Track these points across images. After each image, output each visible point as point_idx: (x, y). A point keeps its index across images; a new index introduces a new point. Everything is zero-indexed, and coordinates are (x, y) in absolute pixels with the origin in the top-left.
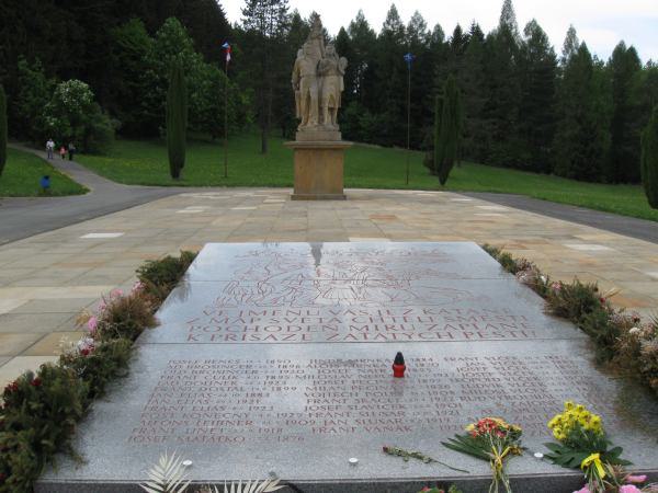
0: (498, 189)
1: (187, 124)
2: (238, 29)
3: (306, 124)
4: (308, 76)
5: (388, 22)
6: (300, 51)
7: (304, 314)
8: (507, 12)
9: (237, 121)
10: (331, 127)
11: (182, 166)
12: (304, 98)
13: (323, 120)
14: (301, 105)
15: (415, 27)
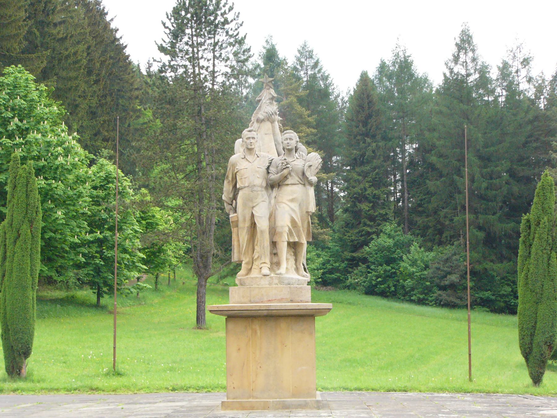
0: (188, 380)
1: (39, 266)
2: (158, 78)
3: (250, 270)
4: (251, 187)
5: (456, 59)
6: (238, 142)
9: (144, 262)
10: (293, 275)
11: (26, 353)
12: (244, 225)
13: (278, 264)
14: (240, 237)
15: (516, 65)
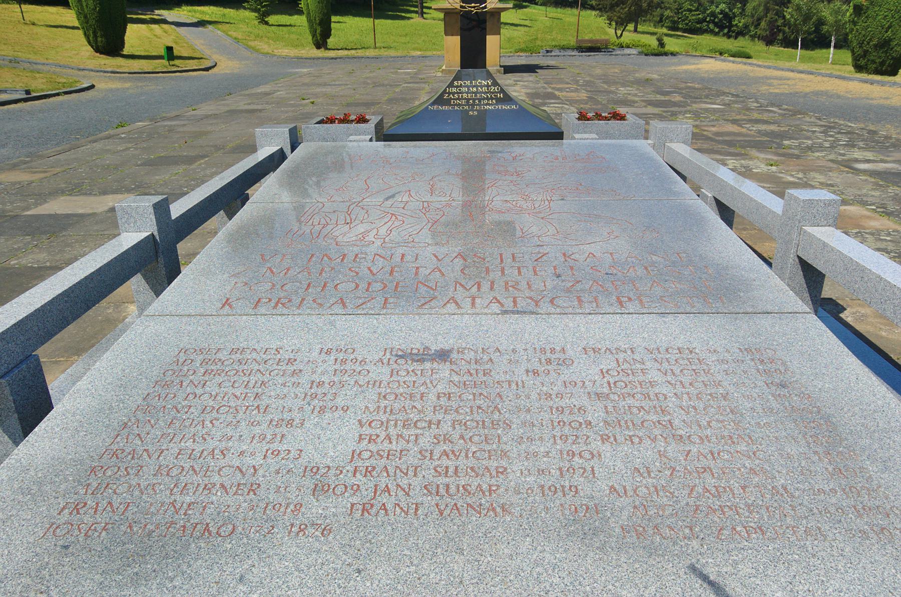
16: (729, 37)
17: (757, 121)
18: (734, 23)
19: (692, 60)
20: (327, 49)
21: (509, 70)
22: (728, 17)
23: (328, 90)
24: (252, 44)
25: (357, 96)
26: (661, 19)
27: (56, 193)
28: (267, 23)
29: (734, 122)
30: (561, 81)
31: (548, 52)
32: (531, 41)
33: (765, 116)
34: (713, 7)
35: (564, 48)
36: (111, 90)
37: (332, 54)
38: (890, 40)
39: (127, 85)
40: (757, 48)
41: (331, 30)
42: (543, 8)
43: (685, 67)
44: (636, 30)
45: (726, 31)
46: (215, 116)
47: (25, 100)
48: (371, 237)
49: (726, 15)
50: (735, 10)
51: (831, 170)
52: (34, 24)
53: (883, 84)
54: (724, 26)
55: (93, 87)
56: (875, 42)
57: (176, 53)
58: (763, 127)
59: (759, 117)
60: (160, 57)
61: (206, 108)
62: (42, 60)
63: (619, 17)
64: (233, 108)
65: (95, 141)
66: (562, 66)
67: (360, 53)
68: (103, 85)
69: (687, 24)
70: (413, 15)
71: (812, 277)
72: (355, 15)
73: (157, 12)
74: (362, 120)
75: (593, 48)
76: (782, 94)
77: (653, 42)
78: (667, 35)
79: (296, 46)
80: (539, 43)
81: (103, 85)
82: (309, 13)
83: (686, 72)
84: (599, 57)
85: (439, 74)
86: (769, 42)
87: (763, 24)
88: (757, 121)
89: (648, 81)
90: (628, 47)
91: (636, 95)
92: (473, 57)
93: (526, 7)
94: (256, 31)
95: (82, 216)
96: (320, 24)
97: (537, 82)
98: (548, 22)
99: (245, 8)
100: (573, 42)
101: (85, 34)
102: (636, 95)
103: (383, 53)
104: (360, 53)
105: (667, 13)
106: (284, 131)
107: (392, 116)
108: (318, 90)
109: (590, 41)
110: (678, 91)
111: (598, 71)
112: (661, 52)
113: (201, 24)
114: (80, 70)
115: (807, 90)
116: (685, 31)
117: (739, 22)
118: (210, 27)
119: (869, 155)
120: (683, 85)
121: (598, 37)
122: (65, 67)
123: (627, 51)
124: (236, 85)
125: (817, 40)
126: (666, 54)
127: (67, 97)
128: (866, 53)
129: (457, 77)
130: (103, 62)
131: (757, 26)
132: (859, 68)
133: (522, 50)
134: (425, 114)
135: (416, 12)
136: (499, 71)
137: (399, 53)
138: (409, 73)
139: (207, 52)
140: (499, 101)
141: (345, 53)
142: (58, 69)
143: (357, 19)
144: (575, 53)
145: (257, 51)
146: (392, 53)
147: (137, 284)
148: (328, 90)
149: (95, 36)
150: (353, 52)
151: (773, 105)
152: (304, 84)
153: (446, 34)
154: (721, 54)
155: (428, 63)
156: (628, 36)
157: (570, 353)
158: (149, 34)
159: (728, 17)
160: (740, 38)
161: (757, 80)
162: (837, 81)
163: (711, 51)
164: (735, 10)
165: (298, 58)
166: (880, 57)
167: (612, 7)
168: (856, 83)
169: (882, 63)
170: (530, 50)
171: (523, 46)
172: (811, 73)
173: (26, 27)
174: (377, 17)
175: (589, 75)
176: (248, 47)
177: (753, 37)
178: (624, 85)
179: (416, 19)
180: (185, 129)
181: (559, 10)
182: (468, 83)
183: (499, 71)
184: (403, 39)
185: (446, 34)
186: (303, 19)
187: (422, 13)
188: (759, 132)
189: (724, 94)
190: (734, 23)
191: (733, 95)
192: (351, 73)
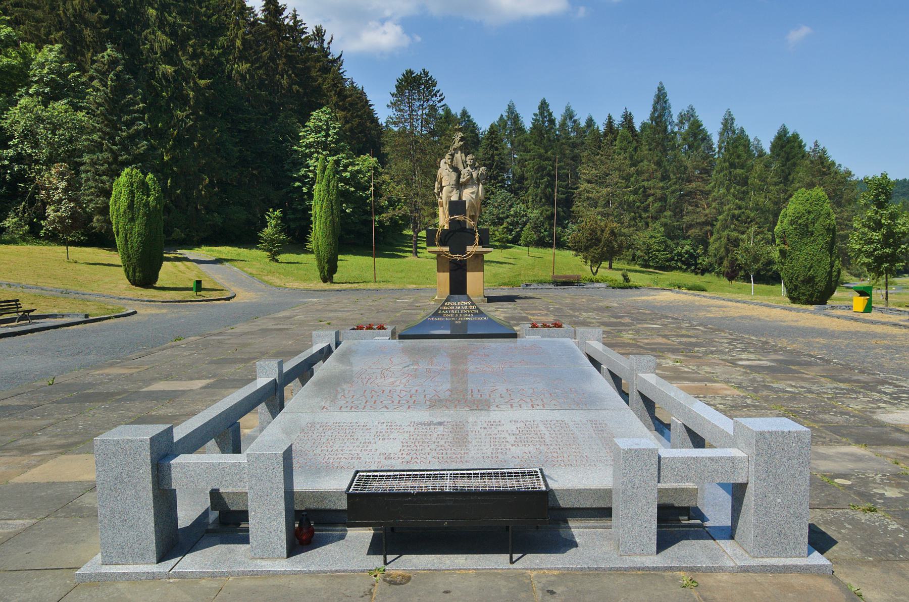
7: (413, 391)
8: (661, 98)
16: (697, 273)
17: (682, 336)
18: (699, 262)
19: (652, 292)
20: (332, 282)
21: (491, 299)
22: (693, 257)
23: (340, 314)
24: (266, 278)
25: (365, 319)
26: (634, 258)
27: (154, 380)
28: (277, 261)
29: (665, 336)
30: (535, 308)
31: (527, 285)
32: (515, 277)
33: (691, 333)
34: (679, 249)
35: (541, 282)
36: (152, 315)
37: (337, 287)
38: (814, 277)
39: (164, 311)
40: (722, 283)
41: (337, 267)
42: (526, 248)
43: (643, 298)
44: (610, 267)
45: (693, 268)
46: (252, 333)
47: (85, 322)
48: (398, 383)
49: (691, 255)
50: (698, 251)
51: (718, 365)
52: (76, 262)
53: (798, 310)
54: (690, 263)
55: (135, 312)
56: (801, 278)
57: (204, 285)
58: (684, 340)
59: (686, 333)
60: (191, 289)
61: (240, 328)
62: (87, 291)
63: (594, 257)
64: (264, 327)
65: (163, 349)
66: (538, 296)
67: (362, 286)
68: (144, 311)
69: (657, 262)
70: (408, 254)
71: (649, 404)
72: (355, 254)
73: (179, 251)
74: (381, 328)
75: (567, 283)
76: (715, 318)
77: (618, 277)
78: (630, 271)
79: (305, 280)
80: (522, 278)
81: (144, 311)
82: (318, 254)
83: (644, 301)
84: (572, 289)
85: (433, 303)
86: (731, 276)
87: (726, 263)
88: (682, 336)
89: (608, 308)
90: (598, 282)
91: (594, 318)
92: (458, 287)
93: (510, 247)
94: (268, 268)
95: (184, 391)
96: (328, 262)
97: (515, 309)
98: (530, 260)
99: (257, 248)
100: (549, 278)
101: (126, 270)
102: (594, 318)
103: (383, 286)
104: (362, 286)
105: (639, 253)
106: (333, 333)
107: (400, 329)
108: (331, 315)
109: (565, 277)
110: (629, 315)
111: (568, 301)
112: (626, 285)
113: (219, 261)
114: (120, 299)
115: (736, 315)
116: (656, 268)
117: (704, 261)
118: (227, 264)
119: (752, 357)
120: (636, 311)
121: (576, 273)
122: (108, 297)
123: (597, 285)
124: (253, 312)
125: (766, 276)
126: (631, 287)
127: (116, 320)
128: (796, 287)
129: (447, 300)
130: (139, 293)
131: (720, 264)
132: (794, 300)
133: (505, 284)
134: (425, 323)
135: (411, 252)
136: (483, 301)
137: (397, 287)
138: (404, 302)
139: (226, 285)
140: (475, 314)
141: (349, 286)
142: (102, 299)
143: (358, 258)
144: (552, 286)
145: (271, 284)
146: (391, 286)
147: (262, 408)
148: (340, 314)
149: (134, 272)
150: (356, 285)
151: (701, 325)
152: (317, 310)
153: (438, 271)
154: (679, 287)
155: (422, 294)
156: (604, 271)
157: (503, 422)
158: (174, 270)
159: (693, 257)
160: (707, 274)
161: (706, 308)
162: (765, 309)
163: (670, 285)
164: (698, 251)
165: (307, 290)
166: (808, 291)
167: (587, 249)
168: (779, 310)
169: (811, 295)
170: (512, 284)
171: (507, 280)
172: (745, 302)
173: (69, 265)
174: (377, 256)
175: (560, 304)
176: (262, 281)
177: (718, 274)
178: (586, 311)
179: (410, 257)
180: (231, 341)
181: (541, 250)
182: (455, 304)
183: (483, 301)
184: (400, 275)
185: (438, 271)
186: (312, 257)
187: (416, 253)
188: (680, 343)
189: (667, 317)
190: (699, 262)
191: (673, 318)
192: (357, 301)
